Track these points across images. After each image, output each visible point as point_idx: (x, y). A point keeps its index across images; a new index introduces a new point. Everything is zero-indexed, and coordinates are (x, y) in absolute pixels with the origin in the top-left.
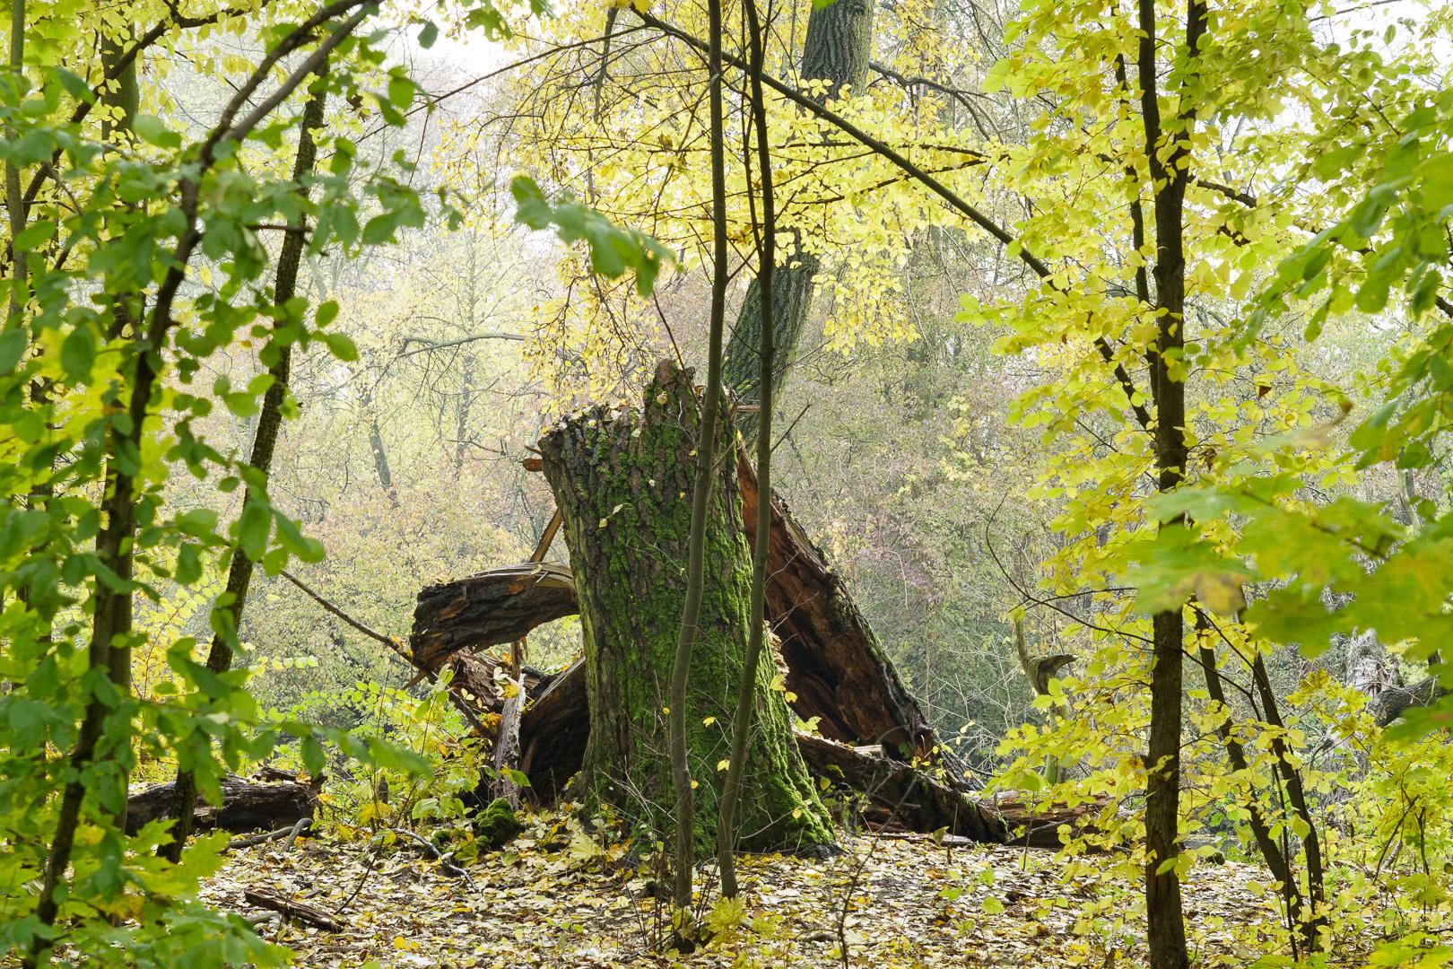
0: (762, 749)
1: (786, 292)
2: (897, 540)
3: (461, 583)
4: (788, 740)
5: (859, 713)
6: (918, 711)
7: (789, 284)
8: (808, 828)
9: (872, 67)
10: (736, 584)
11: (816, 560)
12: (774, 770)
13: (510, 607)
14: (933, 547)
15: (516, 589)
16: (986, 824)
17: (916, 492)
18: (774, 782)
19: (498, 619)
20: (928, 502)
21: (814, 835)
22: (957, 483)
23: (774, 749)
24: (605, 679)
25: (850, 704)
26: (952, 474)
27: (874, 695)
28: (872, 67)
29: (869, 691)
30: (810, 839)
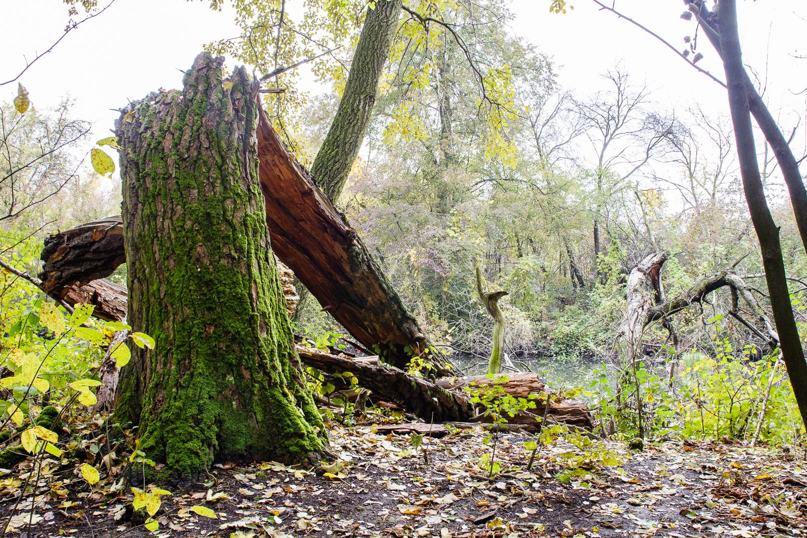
0: (262, 366)
1: (358, 106)
2: (431, 256)
3: (64, 234)
4: (291, 357)
5: (377, 327)
6: (416, 325)
7: (360, 102)
8: (302, 436)
9: (404, 8)
10: (246, 225)
11: (338, 220)
12: (273, 385)
13: (95, 252)
14: (445, 259)
15: (98, 236)
16: (460, 406)
17: (439, 241)
18: (273, 396)
19: (91, 260)
20: (442, 244)
21: (306, 443)
22: (453, 237)
23: (274, 368)
24: (135, 306)
25: (371, 321)
26: (452, 233)
27: (387, 315)
28: (404, 8)
29: (383, 313)
30: (302, 447)
